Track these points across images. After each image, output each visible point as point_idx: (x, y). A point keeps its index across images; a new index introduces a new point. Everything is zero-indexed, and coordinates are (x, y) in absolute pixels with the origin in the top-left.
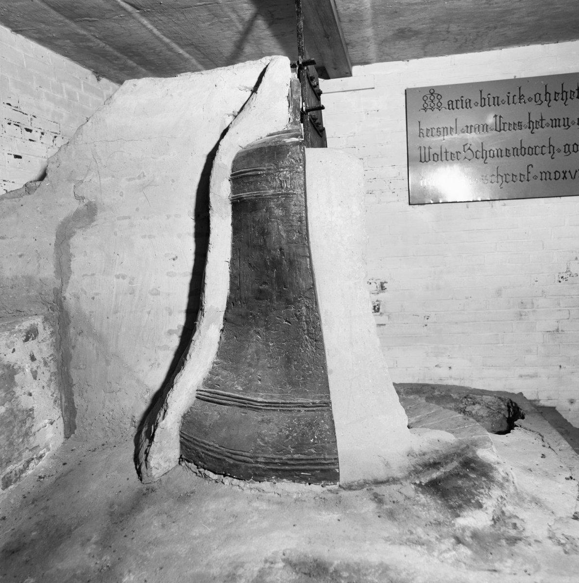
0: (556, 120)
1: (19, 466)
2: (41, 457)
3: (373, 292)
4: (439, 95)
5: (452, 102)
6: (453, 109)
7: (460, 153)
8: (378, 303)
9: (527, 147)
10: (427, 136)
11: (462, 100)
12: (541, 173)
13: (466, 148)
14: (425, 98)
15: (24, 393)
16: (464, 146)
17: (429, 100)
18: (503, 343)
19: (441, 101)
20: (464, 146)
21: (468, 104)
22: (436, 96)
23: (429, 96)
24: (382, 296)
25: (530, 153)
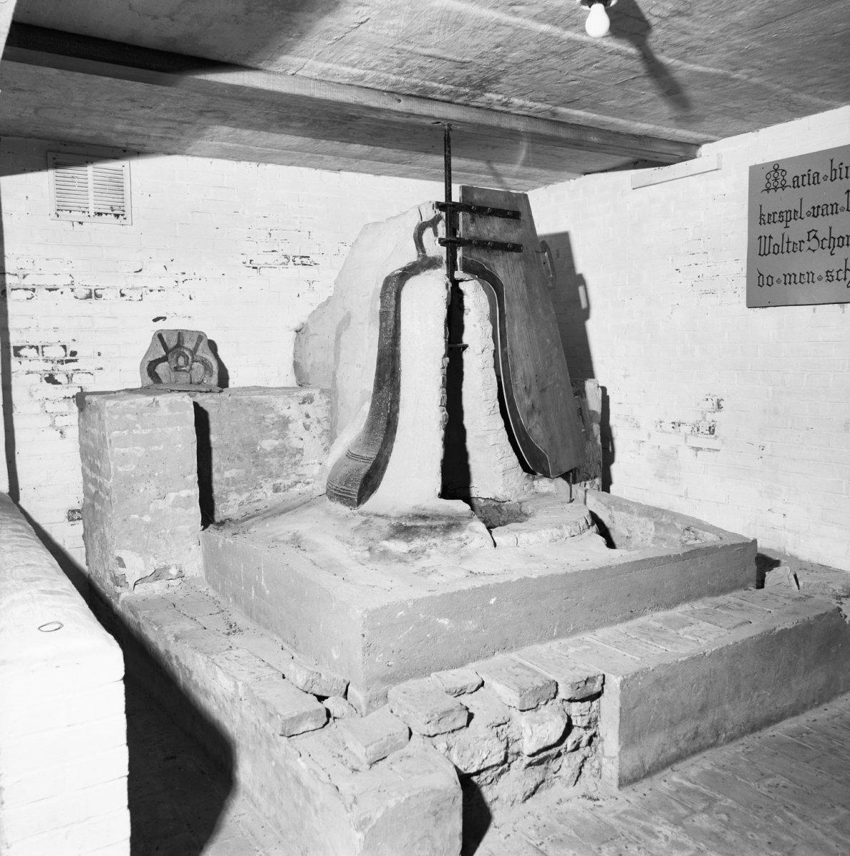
0: (832, 205)
1: (288, 482)
2: (308, 483)
3: (710, 410)
4: (784, 170)
5: (798, 177)
6: (799, 187)
7: (804, 242)
8: (713, 423)
9: (836, 237)
10: (769, 222)
11: (809, 175)
12: (785, 276)
13: (812, 234)
14: (768, 176)
15: (296, 437)
16: (809, 233)
17: (772, 178)
18: (847, 495)
19: (785, 178)
20: (809, 233)
21: (816, 179)
22: (780, 172)
23: (772, 173)
24: (718, 416)
25: (776, 251)
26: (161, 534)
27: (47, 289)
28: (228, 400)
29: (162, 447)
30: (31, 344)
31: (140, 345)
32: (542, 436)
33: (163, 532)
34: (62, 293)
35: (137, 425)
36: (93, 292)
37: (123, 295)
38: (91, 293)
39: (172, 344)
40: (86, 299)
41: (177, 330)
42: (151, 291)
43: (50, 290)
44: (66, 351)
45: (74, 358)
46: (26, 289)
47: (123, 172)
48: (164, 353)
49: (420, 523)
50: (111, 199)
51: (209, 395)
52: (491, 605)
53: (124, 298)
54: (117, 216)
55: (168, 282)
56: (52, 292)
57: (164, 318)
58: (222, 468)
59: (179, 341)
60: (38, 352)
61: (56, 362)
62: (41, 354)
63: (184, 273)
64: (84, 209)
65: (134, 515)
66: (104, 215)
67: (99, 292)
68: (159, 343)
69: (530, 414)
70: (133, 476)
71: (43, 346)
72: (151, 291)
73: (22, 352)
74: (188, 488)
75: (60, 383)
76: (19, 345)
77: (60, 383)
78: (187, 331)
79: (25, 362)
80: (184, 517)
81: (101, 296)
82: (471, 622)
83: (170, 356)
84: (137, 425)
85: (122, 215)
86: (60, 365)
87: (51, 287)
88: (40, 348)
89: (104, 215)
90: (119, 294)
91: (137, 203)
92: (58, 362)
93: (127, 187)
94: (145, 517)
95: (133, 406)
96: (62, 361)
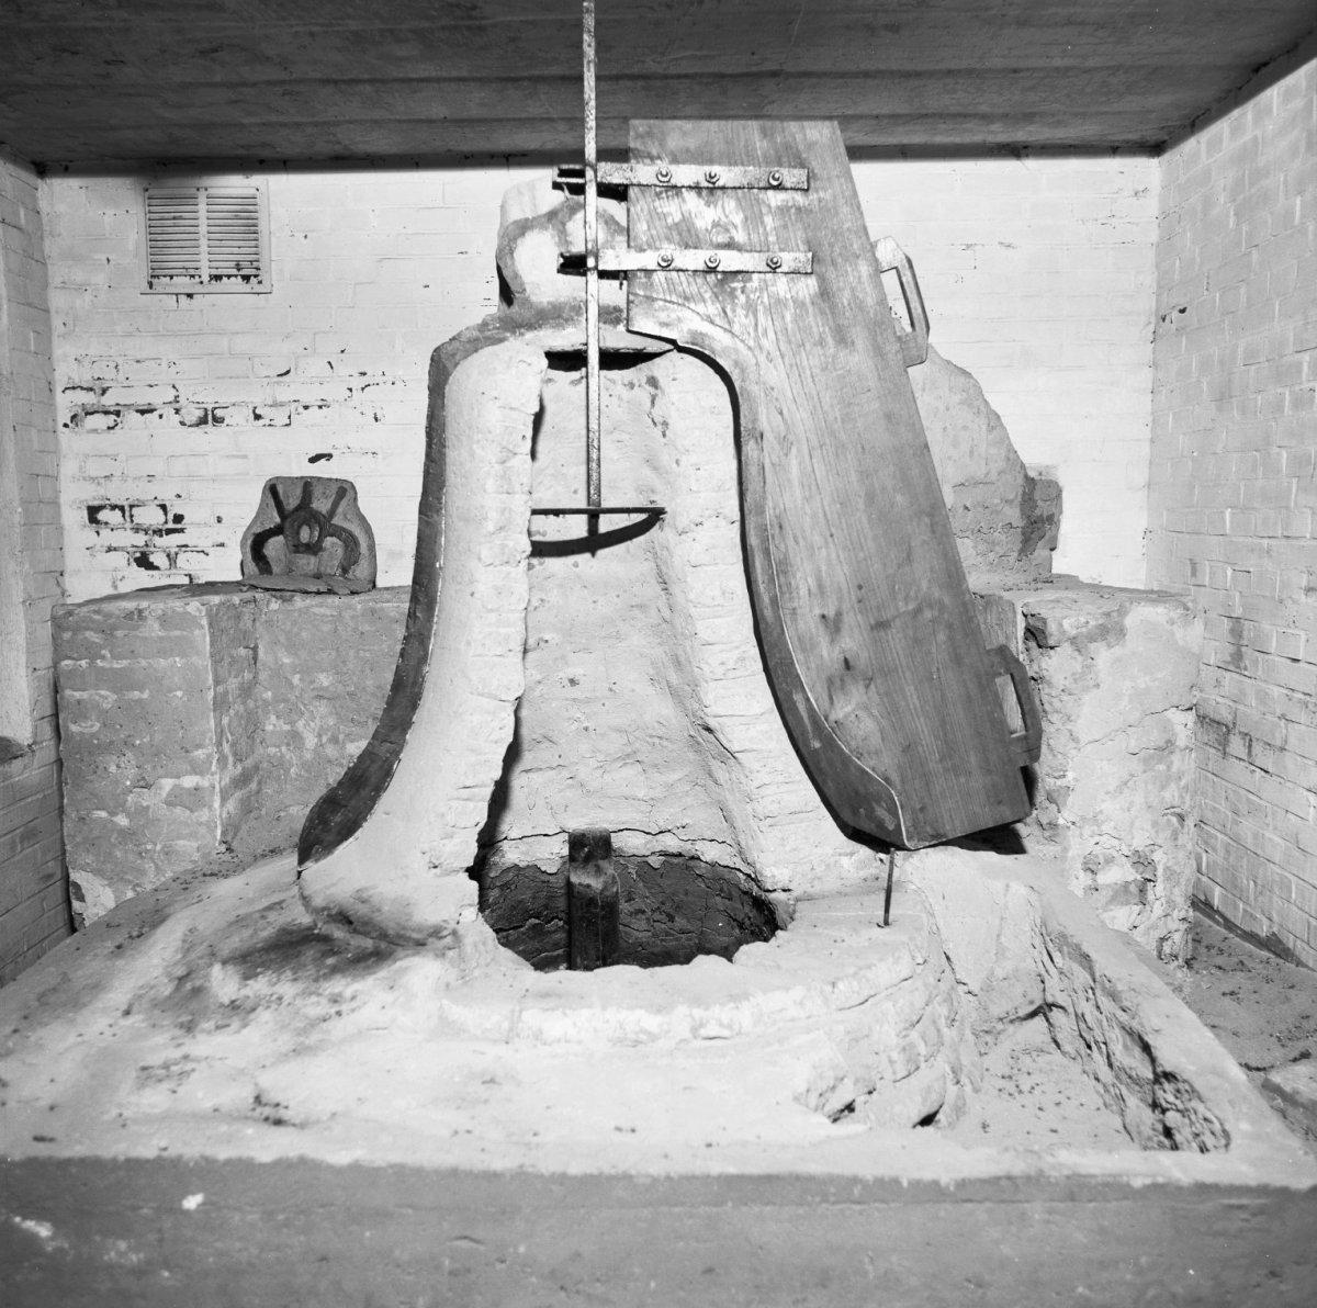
26: (147, 851)
27: (137, 411)
28: (355, 610)
29: (145, 695)
30: (114, 501)
31: (244, 508)
32: (875, 741)
33: (149, 847)
34: (161, 416)
35: (103, 652)
36: (210, 413)
37: (258, 417)
38: (206, 415)
39: (292, 503)
40: (197, 425)
41: (302, 478)
42: (306, 408)
43: (143, 412)
44: (166, 514)
45: (179, 526)
46: (107, 413)
47: (258, 201)
48: (278, 520)
49: (339, 933)
50: (236, 250)
51: (319, 599)
52: (187, 1213)
53: (261, 422)
54: (246, 278)
55: (333, 392)
56: (147, 415)
57: (329, 456)
58: (341, 737)
59: (303, 498)
60: (124, 516)
61: (150, 532)
62: (128, 520)
63: (364, 374)
64: (192, 272)
65: (99, 812)
66: (225, 279)
67: (219, 413)
68: (272, 502)
69: (834, 685)
70: (96, 742)
71: (131, 507)
72: (306, 408)
73: (102, 516)
74: (196, 774)
75: (157, 568)
76: (96, 503)
77: (157, 568)
78: (319, 479)
79: (105, 532)
80: (189, 826)
81: (222, 420)
82: (122, 1245)
83: (287, 525)
84: (103, 652)
85: (256, 276)
86: (156, 538)
87: (146, 408)
88: (127, 508)
89: (225, 279)
90: (252, 416)
91: (281, 251)
92: (154, 532)
93: (263, 226)
94: (120, 816)
95: (97, 617)
96: (160, 530)
